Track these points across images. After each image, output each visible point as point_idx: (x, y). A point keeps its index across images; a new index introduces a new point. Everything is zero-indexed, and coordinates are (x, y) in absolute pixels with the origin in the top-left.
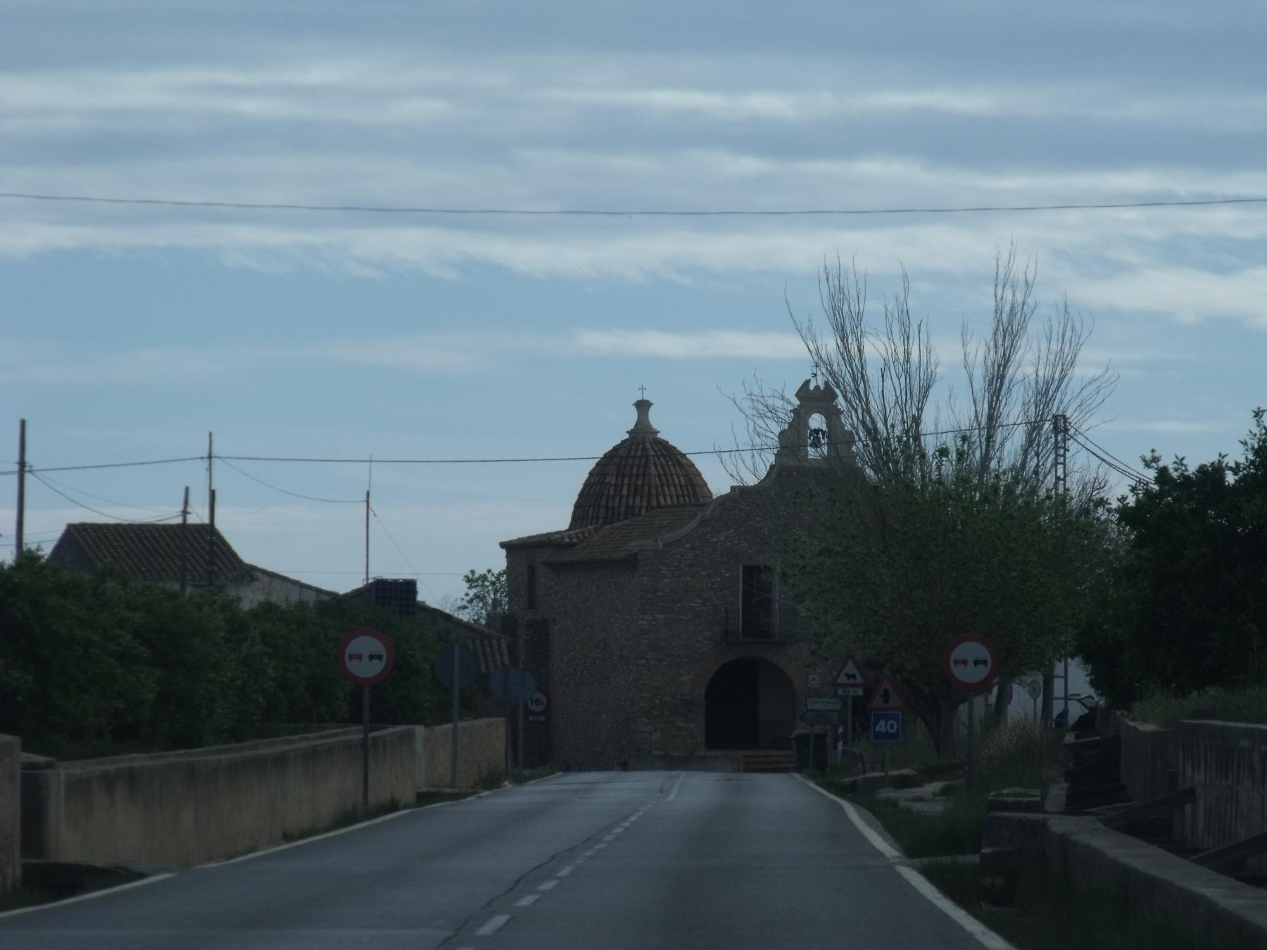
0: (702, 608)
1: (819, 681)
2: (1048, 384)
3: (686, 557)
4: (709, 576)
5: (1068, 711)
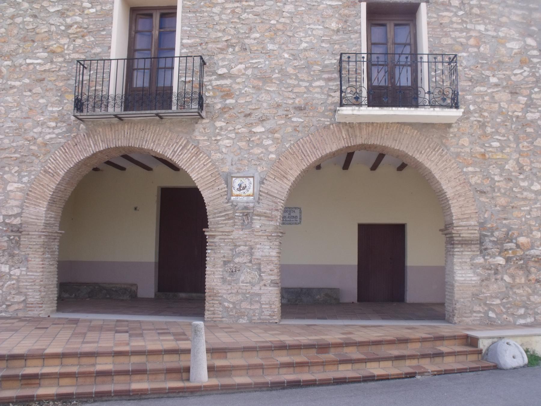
0: (48, 66)
4: (62, 14)
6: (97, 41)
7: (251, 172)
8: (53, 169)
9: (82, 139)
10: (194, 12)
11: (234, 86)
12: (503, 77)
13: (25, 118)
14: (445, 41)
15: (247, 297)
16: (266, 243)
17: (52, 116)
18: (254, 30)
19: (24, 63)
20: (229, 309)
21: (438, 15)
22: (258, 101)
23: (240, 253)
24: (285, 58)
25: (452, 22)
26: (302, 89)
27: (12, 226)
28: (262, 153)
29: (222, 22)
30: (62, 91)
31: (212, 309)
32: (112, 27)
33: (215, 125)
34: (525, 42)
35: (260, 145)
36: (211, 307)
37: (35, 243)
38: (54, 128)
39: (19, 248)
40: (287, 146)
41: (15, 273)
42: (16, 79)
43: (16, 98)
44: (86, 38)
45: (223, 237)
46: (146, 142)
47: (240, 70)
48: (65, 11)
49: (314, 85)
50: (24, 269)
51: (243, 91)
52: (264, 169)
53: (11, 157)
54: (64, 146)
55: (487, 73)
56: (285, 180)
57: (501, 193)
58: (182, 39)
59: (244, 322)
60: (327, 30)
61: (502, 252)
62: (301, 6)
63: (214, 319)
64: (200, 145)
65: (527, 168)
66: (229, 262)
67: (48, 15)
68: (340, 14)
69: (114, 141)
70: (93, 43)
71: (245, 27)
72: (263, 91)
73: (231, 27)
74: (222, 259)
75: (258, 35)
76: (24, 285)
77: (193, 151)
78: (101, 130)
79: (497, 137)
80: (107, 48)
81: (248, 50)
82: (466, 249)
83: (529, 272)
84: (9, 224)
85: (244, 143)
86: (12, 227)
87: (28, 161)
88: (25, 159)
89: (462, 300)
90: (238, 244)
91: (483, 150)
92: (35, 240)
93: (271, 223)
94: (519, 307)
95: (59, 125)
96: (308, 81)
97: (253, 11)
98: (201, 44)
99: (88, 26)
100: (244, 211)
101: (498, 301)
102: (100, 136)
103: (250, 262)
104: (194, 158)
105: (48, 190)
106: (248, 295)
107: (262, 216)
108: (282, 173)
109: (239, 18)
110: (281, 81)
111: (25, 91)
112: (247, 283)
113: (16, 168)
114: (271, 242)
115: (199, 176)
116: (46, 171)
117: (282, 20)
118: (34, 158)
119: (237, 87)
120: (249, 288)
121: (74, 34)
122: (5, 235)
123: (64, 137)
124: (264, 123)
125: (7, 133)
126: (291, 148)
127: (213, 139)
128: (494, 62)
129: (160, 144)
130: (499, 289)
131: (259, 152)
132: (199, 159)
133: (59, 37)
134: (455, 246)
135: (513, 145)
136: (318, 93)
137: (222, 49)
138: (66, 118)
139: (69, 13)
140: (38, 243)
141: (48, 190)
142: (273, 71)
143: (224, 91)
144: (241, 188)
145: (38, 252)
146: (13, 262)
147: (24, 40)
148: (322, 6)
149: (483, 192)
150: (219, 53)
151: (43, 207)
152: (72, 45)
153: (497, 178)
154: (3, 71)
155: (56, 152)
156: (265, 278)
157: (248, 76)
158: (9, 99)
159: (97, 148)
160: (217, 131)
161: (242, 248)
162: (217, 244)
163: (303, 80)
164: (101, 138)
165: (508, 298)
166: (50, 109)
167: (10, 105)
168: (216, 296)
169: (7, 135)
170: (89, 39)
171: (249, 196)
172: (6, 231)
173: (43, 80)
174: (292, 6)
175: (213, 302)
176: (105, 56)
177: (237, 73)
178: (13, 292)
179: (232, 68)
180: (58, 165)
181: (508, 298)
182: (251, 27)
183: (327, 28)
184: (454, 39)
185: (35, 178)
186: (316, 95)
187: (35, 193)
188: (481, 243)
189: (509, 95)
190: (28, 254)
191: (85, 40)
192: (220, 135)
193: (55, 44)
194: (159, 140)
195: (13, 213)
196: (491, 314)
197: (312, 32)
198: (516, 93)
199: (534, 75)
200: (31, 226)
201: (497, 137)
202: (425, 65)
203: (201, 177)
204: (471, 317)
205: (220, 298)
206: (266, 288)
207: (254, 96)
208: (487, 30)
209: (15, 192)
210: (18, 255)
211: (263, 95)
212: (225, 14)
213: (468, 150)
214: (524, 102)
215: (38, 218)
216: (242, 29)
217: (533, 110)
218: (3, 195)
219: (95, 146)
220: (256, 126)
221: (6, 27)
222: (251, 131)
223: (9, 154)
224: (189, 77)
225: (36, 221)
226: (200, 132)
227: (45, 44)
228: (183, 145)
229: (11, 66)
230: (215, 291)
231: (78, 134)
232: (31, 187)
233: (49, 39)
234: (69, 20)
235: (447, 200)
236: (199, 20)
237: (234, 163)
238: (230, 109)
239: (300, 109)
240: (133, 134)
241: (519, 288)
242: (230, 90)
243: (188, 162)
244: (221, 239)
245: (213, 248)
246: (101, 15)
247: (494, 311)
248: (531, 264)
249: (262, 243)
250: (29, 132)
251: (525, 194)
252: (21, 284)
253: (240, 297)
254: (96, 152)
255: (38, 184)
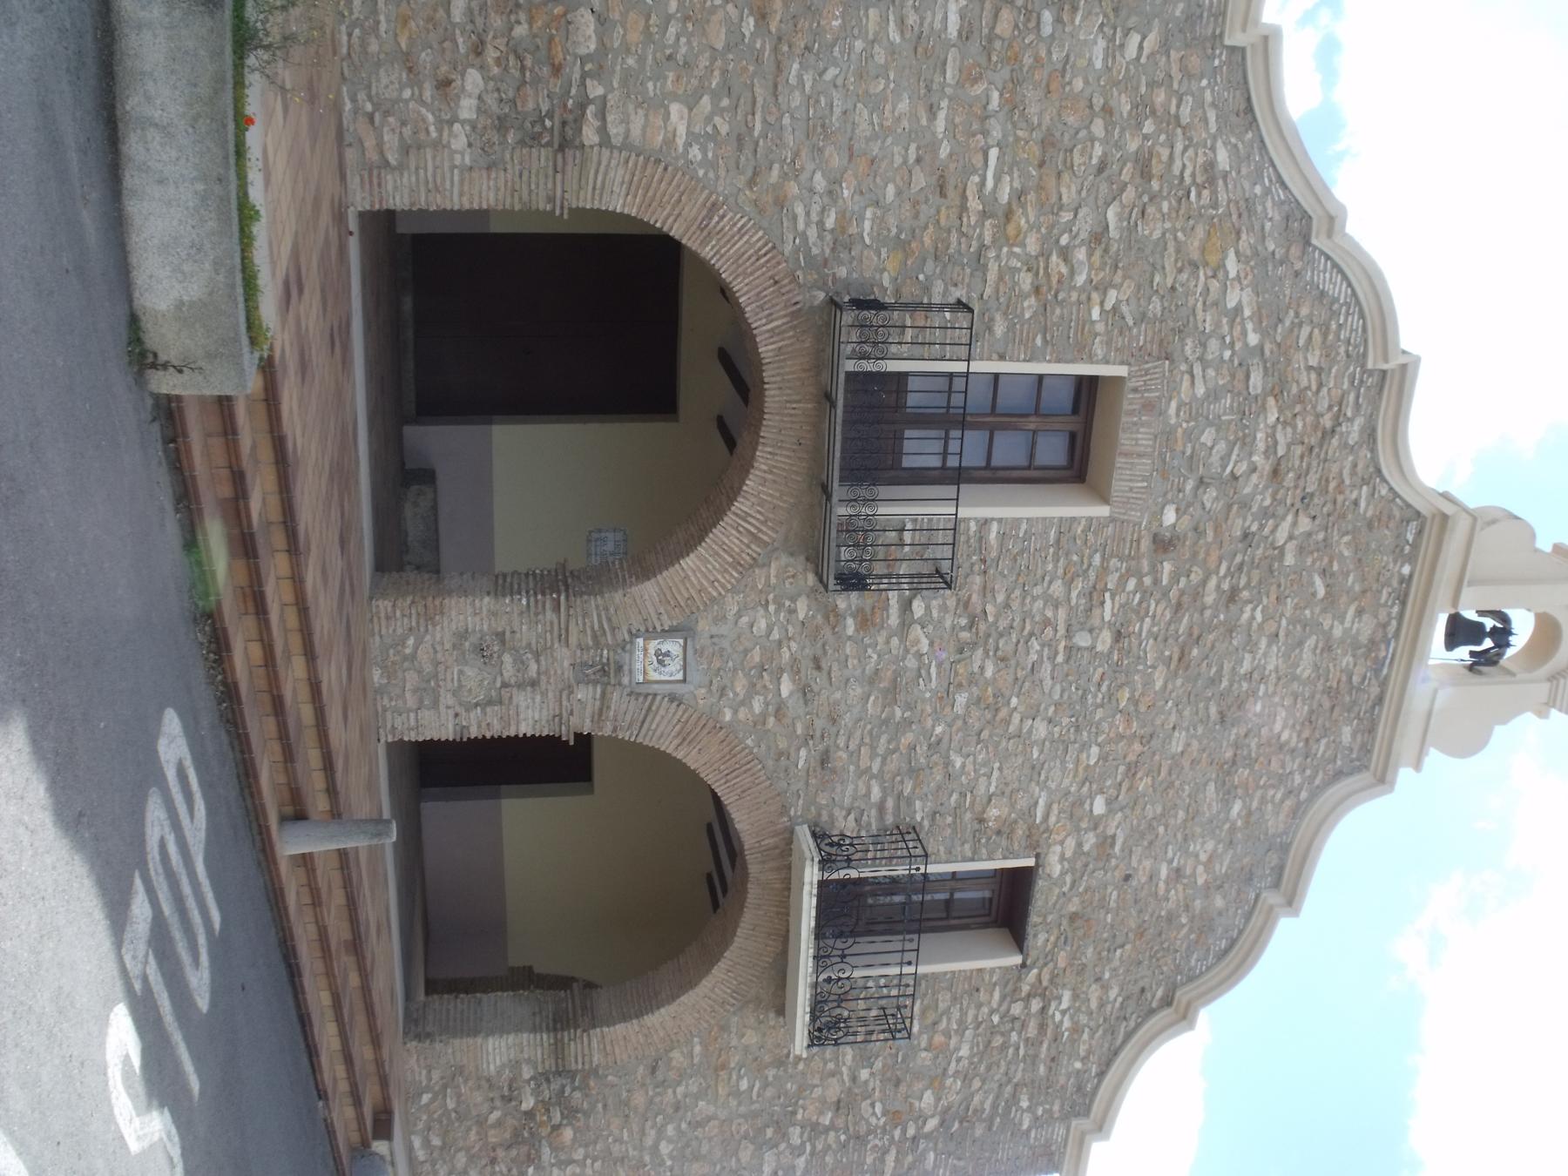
0: (974, 204)
1: (654, 676)
2: (289, 784)
3: (1179, 147)
4: (1099, 237)
5: (140, 313)
6: (1022, 325)
7: (695, 677)
8: (718, 228)
9: (789, 300)
10: (1058, 541)
11: (884, 633)
12: (870, 1088)
13: (850, 148)
14: (944, 1000)
15: (429, 681)
16: (545, 713)
17: (851, 219)
18: (1002, 665)
19: (990, 142)
20: (400, 648)
21: (995, 984)
22: (848, 680)
23: (523, 662)
24: (933, 726)
25: (979, 1006)
26: (864, 762)
27: (580, 119)
28: (736, 694)
29: (1028, 601)
30: (909, 243)
31: (398, 613)
32: (1049, 361)
33: (799, 595)
34: (932, 1116)
35: (752, 689)
36: (402, 611)
37: (533, 187)
38: (820, 224)
39: (522, 143)
40: (749, 742)
41: (456, 136)
42: (953, 120)
43: (905, 123)
44: (1033, 300)
45: (556, 628)
46: (770, 453)
47: (917, 642)
48: (1103, 246)
49: (873, 782)
50: (467, 160)
51: (870, 650)
52: (701, 702)
53: (753, 114)
54: (775, 251)
55: (878, 1064)
56: (676, 742)
57: (652, 1097)
58: (1000, 521)
59: (376, 679)
60: (985, 800)
61: (546, 1106)
62: (1041, 752)
63: (375, 620)
64: (757, 571)
65: (699, 1132)
66: (503, 642)
67: (1100, 203)
68: (1015, 822)
69: (778, 379)
70: (1016, 316)
71: (1010, 648)
72: (866, 689)
73: (1013, 620)
74: (508, 628)
75: (989, 673)
76: (426, 161)
77: (744, 555)
78: (807, 345)
79: (757, 1085)
80: (1001, 351)
81: (958, 656)
82: (546, 1052)
83: (509, 1147)
84: (584, 114)
85: (757, 659)
86: (575, 121)
87: (743, 159)
88: (748, 151)
89: (450, 1051)
90: (542, 658)
91: (732, 1065)
92: (542, 186)
93: (588, 721)
94: (445, 1134)
95: (829, 237)
96: (881, 770)
97: (1042, 661)
98: (984, 561)
99: (1061, 304)
100: (612, 666)
101: (451, 1104)
102: (792, 344)
103: (505, 685)
104: (731, 560)
105: (667, 218)
106: (432, 683)
107: (602, 704)
108: (692, 736)
109: (1031, 634)
110: (886, 722)
111: (918, 148)
112: (459, 680)
113: (724, 129)
114: (548, 721)
115: (690, 573)
116: (715, 206)
117: (1016, 718)
118: (749, 173)
119: (881, 640)
120: (449, 685)
121: (1046, 268)
122: (553, 105)
123: (797, 250)
124: (800, 695)
125: (818, 101)
126: (743, 749)
127: (771, 596)
128: (898, 1073)
129: (763, 485)
130: (475, 1105)
131: (738, 690)
132: (726, 571)
133: (1043, 230)
134: (552, 1035)
135: (742, 1109)
136: (856, 790)
137: (967, 604)
138: (844, 256)
139: (1098, 253)
140: (534, 197)
141: (667, 218)
142: (909, 706)
143: (873, 613)
144: (662, 658)
145: (513, 196)
146: (485, 128)
147: (1047, 143)
148: (1037, 789)
149: (654, 1070)
150: (959, 600)
151: (624, 205)
152: (1019, 265)
153: (680, 1090)
154: (976, 87)
155: (761, 233)
156: (472, 715)
157: (904, 659)
158: (904, 106)
159: (763, 337)
160: (787, 603)
161: (533, 667)
162: (540, 617)
163: (884, 762)
164: (786, 346)
165: (458, 1119)
166: (869, 214)
167: (888, 107)
168: (426, 620)
169: (812, 102)
170: (1030, 307)
171: (645, 673)
172: (565, 105)
173: (943, 194)
174: (1043, 736)
175: (414, 617)
176: (983, 346)
177: (911, 637)
178: (407, 131)
179: (923, 628)
180: (729, 241)
181: (458, 1119)
182: (1008, 660)
183: (990, 800)
184: (947, 1012)
185: (699, 180)
186: (851, 787)
187: (661, 181)
188: (558, 1073)
189: (835, 1099)
190: (505, 170)
191: (1027, 296)
192: (777, 611)
193: (1027, 221)
194: (775, 482)
195: (609, 125)
196: (426, 1098)
197: (984, 775)
198: (838, 1109)
199: (869, 1132)
200: (576, 174)
201: (757, 1085)
202: (895, 971)
203: (687, 577)
204: (419, 1066)
205: (422, 629)
206: (451, 718)
207: (858, 672)
208: (959, 1060)
209: (666, 128)
210: (503, 143)
211: (859, 690)
212: (1045, 605)
213: (734, 1042)
214: (821, 1120)
215: (597, 192)
216: (1006, 643)
217: (806, 1135)
218: (658, 92)
219: (768, 331)
220: (794, 681)
221: (1087, 94)
222: (781, 670)
223: (763, 107)
224: (913, 538)
225: (590, 188)
226: (787, 566)
227: (1031, 197)
228: (760, 535)
229: (985, 108)
230: (437, 617)
231: (800, 286)
232: (676, 170)
233: (1041, 205)
234: (1081, 254)
235: (639, 1015)
236: (1037, 554)
237: (715, 640)
238: (834, 628)
239: (824, 759)
240: (793, 422)
241: (478, 1133)
242: (874, 625)
243: (720, 546)
244: (552, 623)
245: (533, 609)
246: (1082, 333)
247: (432, 1101)
248: (525, 1149)
249: (545, 706)
250: (814, 160)
251: (653, 1132)
252: (429, 153)
253: (428, 668)
254: (755, 336)
255: (682, 188)
